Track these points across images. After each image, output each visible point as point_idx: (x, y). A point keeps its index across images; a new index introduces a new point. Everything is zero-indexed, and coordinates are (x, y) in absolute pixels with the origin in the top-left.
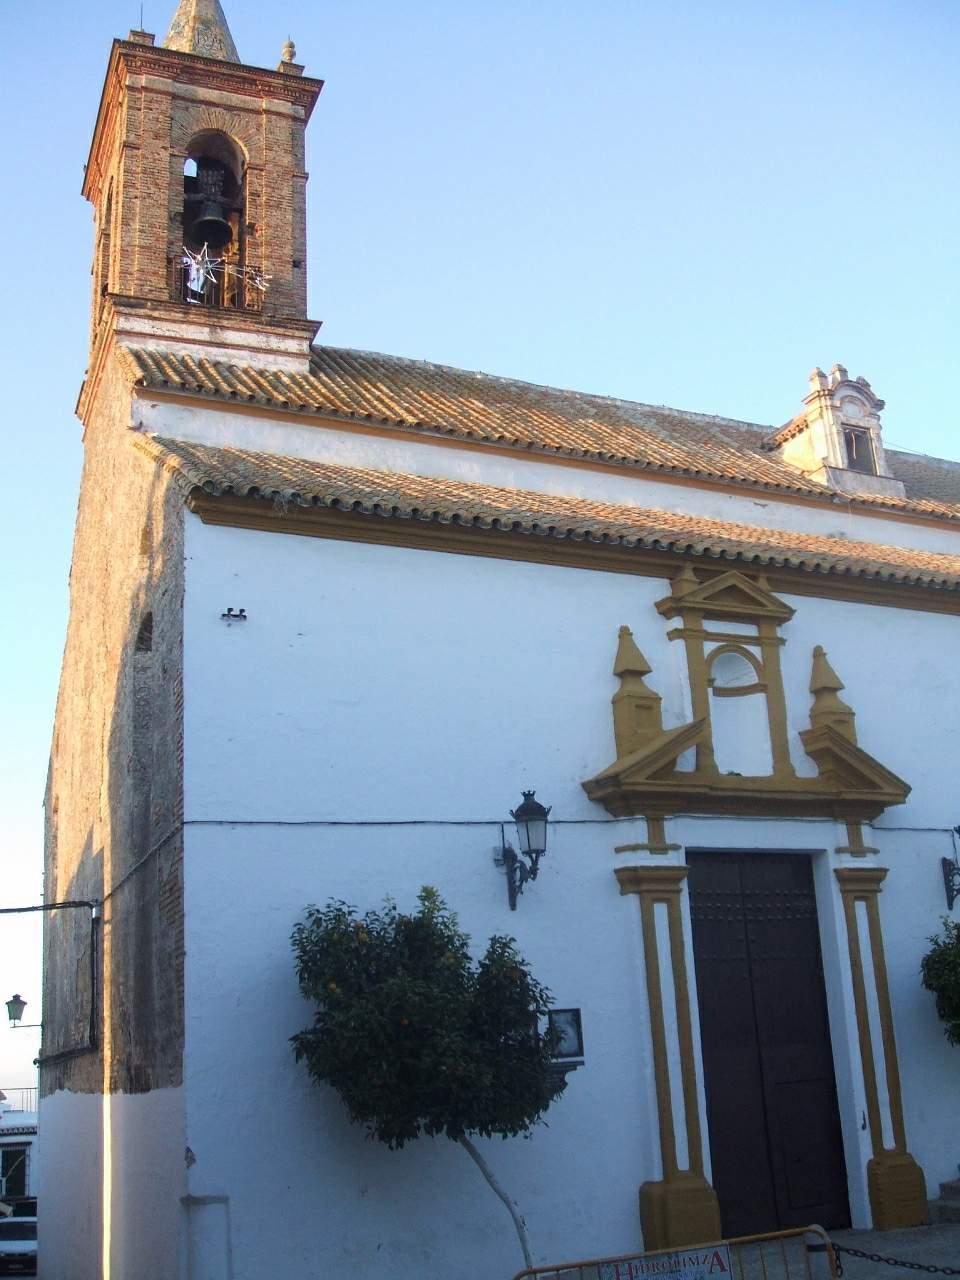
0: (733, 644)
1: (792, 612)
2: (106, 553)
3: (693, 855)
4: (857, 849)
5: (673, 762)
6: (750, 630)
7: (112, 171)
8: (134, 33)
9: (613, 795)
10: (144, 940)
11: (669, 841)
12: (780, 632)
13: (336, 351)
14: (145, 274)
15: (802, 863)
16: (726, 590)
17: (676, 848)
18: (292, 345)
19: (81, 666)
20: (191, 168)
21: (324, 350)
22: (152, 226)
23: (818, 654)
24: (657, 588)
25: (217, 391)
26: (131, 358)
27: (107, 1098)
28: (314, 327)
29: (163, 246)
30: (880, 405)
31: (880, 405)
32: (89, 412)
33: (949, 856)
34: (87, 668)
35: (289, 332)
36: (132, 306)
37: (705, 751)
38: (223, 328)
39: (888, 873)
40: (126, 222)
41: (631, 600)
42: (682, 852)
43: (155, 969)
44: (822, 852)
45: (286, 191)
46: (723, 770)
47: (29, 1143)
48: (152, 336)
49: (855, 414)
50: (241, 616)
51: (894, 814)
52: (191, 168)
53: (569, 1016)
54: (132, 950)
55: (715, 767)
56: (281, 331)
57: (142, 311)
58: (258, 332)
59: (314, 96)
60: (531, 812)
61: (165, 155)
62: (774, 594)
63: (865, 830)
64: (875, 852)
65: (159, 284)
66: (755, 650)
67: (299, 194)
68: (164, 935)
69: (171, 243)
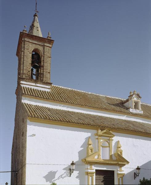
3: (96, 170)
15: (113, 172)
36: (23, 79)
38: (37, 83)
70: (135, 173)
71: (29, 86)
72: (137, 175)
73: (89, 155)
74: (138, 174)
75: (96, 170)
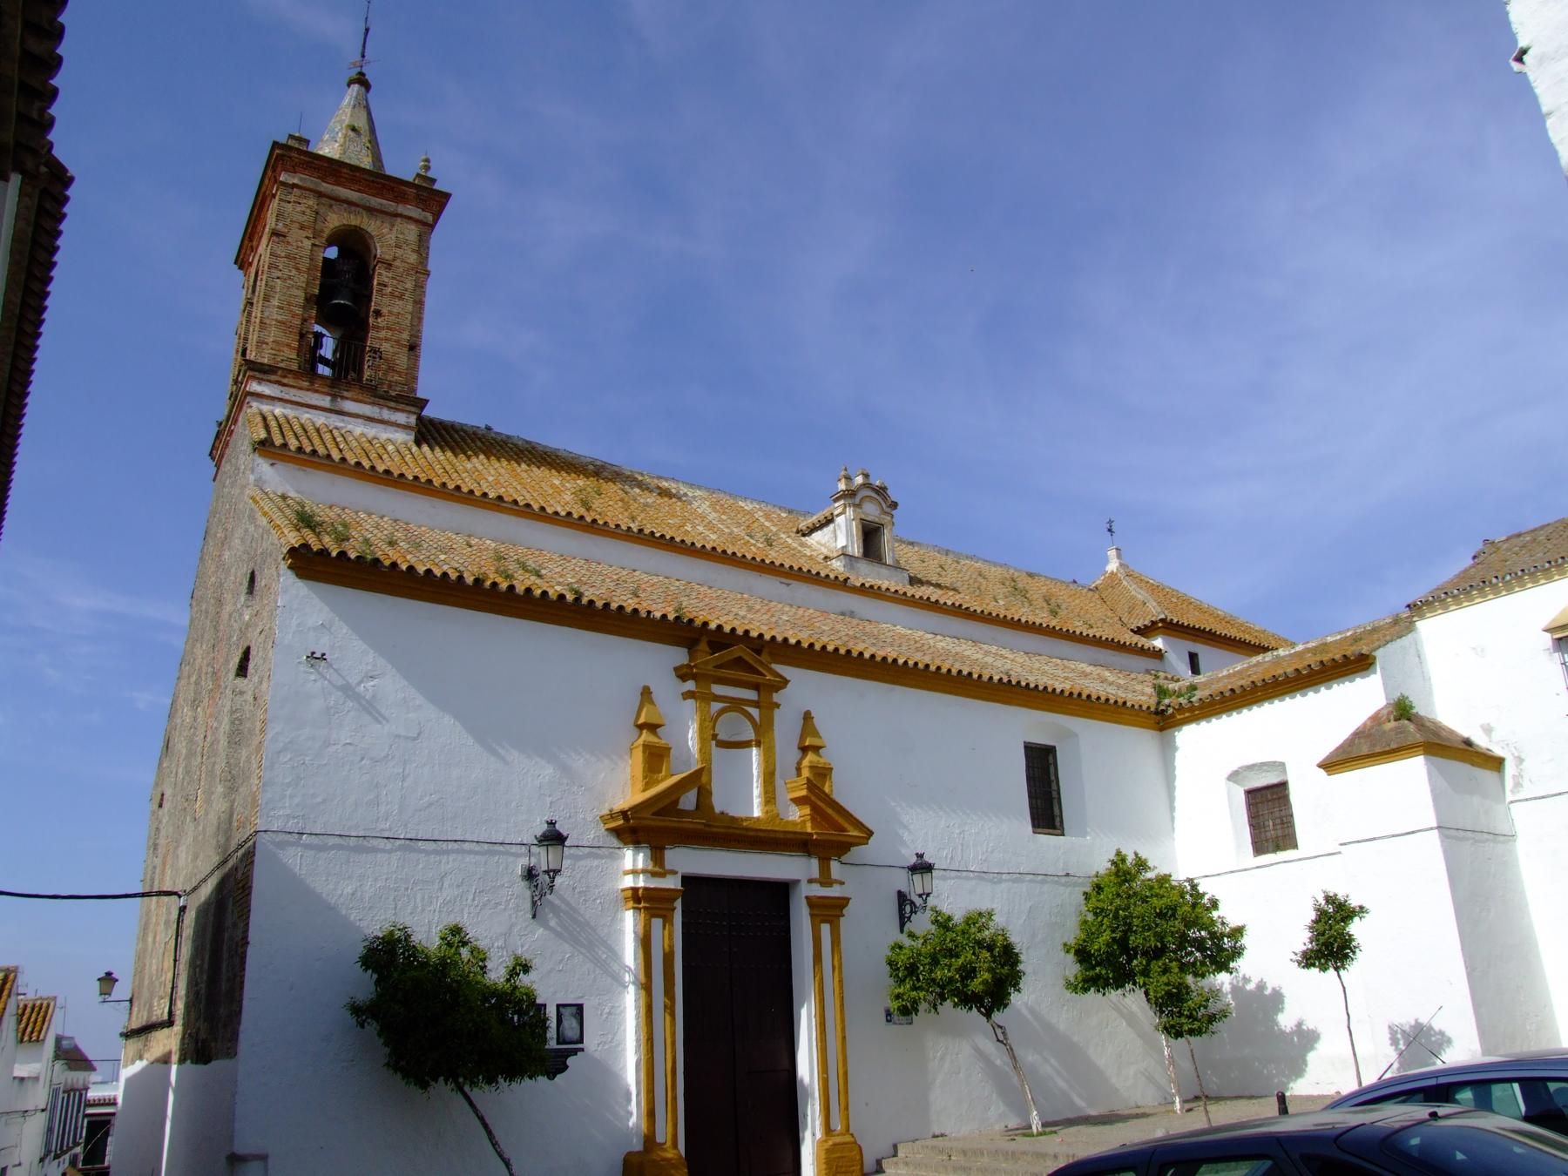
0: (736, 705)
1: (786, 682)
2: (221, 584)
3: (687, 880)
4: (826, 880)
5: (676, 802)
6: (751, 695)
7: (261, 249)
8: (291, 137)
9: (633, 828)
10: (219, 929)
11: (668, 866)
12: (776, 697)
13: (441, 423)
14: (278, 347)
15: (780, 892)
16: (732, 663)
17: (674, 872)
18: (401, 418)
19: (193, 679)
20: (332, 253)
21: (431, 421)
22: (289, 304)
23: (807, 717)
24: (679, 656)
25: (329, 456)
26: (259, 419)
27: (174, 1068)
28: (423, 403)
29: (297, 322)
30: (894, 505)
31: (894, 505)
32: (221, 456)
33: (904, 889)
34: (197, 683)
35: (401, 406)
36: (265, 372)
37: (704, 794)
38: (343, 398)
39: (472, 932)
40: (267, 298)
41: (656, 664)
42: (679, 877)
43: (225, 956)
44: (798, 881)
45: (409, 285)
46: (717, 810)
47: (113, 1114)
48: (280, 400)
49: (872, 511)
50: (323, 657)
51: (856, 853)
52: (332, 253)
53: (574, 1010)
54: (209, 936)
55: (712, 808)
56: (392, 404)
57: (273, 377)
58: (373, 404)
59: (443, 206)
60: (553, 838)
61: (307, 244)
62: (774, 666)
63: (834, 865)
64: (842, 883)
65: (289, 356)
66: (754, 712)
67: (420, 287)
68: (235, 925)
69: (304, 320)
70: (900, 893)
71: (290, 412)
72: (912, 903)
73: (467, 1088)
74: (918, 901)
75: (687, 880)
